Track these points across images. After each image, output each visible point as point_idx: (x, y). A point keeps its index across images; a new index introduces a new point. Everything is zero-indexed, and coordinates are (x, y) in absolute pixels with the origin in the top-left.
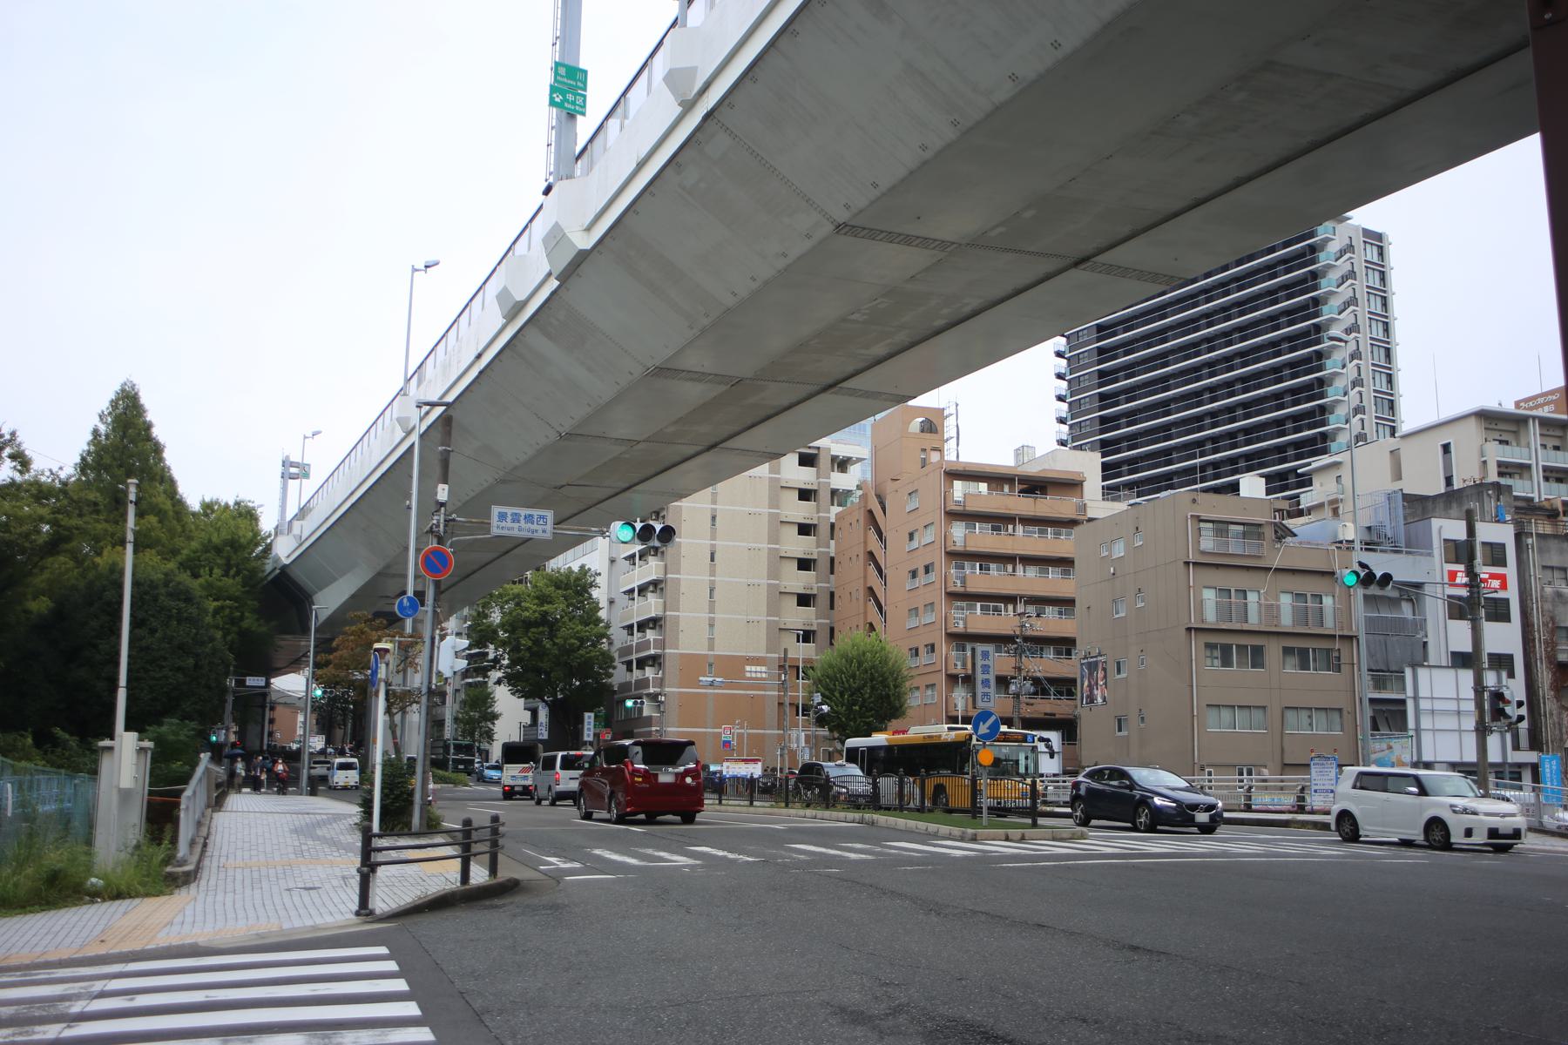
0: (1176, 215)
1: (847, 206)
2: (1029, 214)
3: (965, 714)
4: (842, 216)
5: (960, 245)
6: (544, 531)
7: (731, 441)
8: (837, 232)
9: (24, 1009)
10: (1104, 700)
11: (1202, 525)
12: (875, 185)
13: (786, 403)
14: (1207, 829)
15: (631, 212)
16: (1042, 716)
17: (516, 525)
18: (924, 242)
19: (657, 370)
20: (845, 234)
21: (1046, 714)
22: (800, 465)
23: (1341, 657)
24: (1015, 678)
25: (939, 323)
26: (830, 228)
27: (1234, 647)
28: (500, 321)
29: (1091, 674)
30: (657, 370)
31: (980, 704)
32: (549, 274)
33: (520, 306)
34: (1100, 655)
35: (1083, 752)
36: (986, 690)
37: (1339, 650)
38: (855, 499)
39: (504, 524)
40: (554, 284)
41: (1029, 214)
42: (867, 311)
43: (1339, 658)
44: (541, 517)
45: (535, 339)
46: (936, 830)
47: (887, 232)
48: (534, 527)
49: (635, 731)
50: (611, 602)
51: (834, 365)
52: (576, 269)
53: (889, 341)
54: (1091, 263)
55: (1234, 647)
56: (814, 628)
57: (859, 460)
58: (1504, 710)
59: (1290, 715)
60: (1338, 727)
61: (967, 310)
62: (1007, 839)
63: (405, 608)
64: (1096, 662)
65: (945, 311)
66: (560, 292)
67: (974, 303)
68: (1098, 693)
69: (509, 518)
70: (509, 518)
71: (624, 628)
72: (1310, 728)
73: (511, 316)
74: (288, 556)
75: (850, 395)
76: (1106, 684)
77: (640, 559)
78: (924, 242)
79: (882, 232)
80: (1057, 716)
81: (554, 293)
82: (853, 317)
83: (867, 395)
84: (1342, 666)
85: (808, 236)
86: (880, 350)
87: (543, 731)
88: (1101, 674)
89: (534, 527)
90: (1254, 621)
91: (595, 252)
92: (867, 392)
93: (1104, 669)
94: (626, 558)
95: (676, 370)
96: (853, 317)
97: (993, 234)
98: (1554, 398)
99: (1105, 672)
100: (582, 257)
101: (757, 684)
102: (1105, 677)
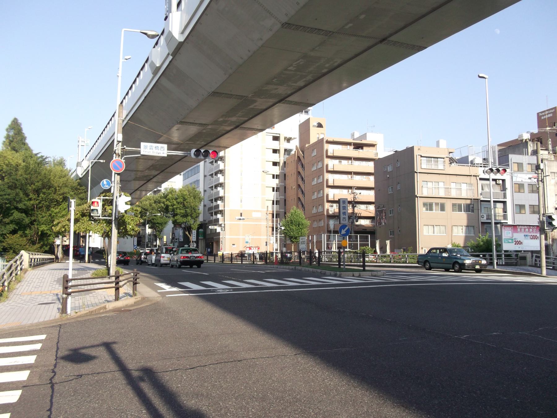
0: (424, 16)
1: (286, 15)
2: (363, 16)
3: (334, 230)
4: (285, 19)
5: (334, 33)
6: (163, 153)
7: (243, 125)
8: (282, 27)
9: (115, 314)
10: (385, 223)
11: (422, 158)
12: (298, 3)
13: (264, 107)
14: (478, 271)
15: (198, 24)
16: (362, 230)
17: (151, 151)
18: (318, 31)
19: (213, 93)
20: (286, 28)
21: (363, 229)
22: (273, 140)
23: (474, 207)
24: (352, 216)
25: (325, 71)
26: (279, 26)
27: (434, 203)
28: (152, 75)
29: (380, 214)
30: (213, 93)
31: (342, 222)
32: (168, 54)
33: (158, 69)
34: (383, 207)
35: (464, 195)
36: (344, 216)
37: (473, 204)
38: (293, 153)
39: (146, 150)
40: (170, 58)
41: (363, 16)
42: (296, 66)
43: (473, 207)
44: (162, 147)
45: (164, 81)
46: (308, 270)
47: (303, 26)
48: (159, 151)
49: (214, 238)
50: (205, 191)
51: (282, 90)
52: (178, 51)
53: (305, 79)
54: (386, 41)
55: (434, 203)
56: (279, 200)
57: (295, 138)
58: (552, 223)
59: (454, 228)
60: (473, 233)
61: (336, 64)
62: (353, 276)
63: (105, 185)
64: (382, 210)
65: (327, 65)
66: (173, 61)
67: (339, 61)
68: (383, 221)
69: (148, 148)
70: (148, 148)
71: (209, 200)
72: (462, 233)
73: (155, 72)
74: (82, 174)
75: (289, 104)
76: (385, 218)
77: (215, 175)
78: (318, 31)
79: (301, 26)
80: (367, 230)
81: (170, 62)
82: (290, 68)
83: (296, 103)
84: (474, 211)
85: (271, 30)
86: (301, 83)
87: (181, 239)
88: (384, 214)
89: (159, 151)
90: (442, 194)
91: (185, 43)
92: (296, 102)
93: (385, 213)
94: (210, 175)
95: (220, 93)
96: (290, 68)
97: (347, 27)
98: (552, 111)
99: (386, 214)
100: (180, 45)
101: (258, 220)
102: (385, 215)
